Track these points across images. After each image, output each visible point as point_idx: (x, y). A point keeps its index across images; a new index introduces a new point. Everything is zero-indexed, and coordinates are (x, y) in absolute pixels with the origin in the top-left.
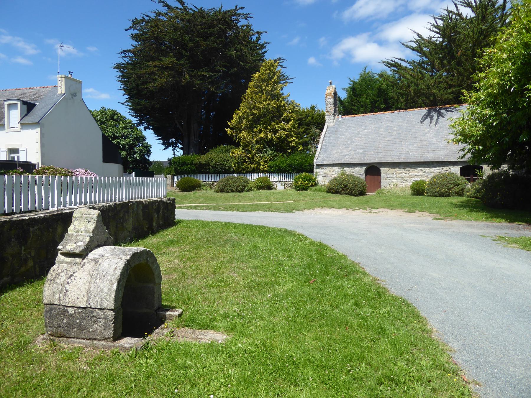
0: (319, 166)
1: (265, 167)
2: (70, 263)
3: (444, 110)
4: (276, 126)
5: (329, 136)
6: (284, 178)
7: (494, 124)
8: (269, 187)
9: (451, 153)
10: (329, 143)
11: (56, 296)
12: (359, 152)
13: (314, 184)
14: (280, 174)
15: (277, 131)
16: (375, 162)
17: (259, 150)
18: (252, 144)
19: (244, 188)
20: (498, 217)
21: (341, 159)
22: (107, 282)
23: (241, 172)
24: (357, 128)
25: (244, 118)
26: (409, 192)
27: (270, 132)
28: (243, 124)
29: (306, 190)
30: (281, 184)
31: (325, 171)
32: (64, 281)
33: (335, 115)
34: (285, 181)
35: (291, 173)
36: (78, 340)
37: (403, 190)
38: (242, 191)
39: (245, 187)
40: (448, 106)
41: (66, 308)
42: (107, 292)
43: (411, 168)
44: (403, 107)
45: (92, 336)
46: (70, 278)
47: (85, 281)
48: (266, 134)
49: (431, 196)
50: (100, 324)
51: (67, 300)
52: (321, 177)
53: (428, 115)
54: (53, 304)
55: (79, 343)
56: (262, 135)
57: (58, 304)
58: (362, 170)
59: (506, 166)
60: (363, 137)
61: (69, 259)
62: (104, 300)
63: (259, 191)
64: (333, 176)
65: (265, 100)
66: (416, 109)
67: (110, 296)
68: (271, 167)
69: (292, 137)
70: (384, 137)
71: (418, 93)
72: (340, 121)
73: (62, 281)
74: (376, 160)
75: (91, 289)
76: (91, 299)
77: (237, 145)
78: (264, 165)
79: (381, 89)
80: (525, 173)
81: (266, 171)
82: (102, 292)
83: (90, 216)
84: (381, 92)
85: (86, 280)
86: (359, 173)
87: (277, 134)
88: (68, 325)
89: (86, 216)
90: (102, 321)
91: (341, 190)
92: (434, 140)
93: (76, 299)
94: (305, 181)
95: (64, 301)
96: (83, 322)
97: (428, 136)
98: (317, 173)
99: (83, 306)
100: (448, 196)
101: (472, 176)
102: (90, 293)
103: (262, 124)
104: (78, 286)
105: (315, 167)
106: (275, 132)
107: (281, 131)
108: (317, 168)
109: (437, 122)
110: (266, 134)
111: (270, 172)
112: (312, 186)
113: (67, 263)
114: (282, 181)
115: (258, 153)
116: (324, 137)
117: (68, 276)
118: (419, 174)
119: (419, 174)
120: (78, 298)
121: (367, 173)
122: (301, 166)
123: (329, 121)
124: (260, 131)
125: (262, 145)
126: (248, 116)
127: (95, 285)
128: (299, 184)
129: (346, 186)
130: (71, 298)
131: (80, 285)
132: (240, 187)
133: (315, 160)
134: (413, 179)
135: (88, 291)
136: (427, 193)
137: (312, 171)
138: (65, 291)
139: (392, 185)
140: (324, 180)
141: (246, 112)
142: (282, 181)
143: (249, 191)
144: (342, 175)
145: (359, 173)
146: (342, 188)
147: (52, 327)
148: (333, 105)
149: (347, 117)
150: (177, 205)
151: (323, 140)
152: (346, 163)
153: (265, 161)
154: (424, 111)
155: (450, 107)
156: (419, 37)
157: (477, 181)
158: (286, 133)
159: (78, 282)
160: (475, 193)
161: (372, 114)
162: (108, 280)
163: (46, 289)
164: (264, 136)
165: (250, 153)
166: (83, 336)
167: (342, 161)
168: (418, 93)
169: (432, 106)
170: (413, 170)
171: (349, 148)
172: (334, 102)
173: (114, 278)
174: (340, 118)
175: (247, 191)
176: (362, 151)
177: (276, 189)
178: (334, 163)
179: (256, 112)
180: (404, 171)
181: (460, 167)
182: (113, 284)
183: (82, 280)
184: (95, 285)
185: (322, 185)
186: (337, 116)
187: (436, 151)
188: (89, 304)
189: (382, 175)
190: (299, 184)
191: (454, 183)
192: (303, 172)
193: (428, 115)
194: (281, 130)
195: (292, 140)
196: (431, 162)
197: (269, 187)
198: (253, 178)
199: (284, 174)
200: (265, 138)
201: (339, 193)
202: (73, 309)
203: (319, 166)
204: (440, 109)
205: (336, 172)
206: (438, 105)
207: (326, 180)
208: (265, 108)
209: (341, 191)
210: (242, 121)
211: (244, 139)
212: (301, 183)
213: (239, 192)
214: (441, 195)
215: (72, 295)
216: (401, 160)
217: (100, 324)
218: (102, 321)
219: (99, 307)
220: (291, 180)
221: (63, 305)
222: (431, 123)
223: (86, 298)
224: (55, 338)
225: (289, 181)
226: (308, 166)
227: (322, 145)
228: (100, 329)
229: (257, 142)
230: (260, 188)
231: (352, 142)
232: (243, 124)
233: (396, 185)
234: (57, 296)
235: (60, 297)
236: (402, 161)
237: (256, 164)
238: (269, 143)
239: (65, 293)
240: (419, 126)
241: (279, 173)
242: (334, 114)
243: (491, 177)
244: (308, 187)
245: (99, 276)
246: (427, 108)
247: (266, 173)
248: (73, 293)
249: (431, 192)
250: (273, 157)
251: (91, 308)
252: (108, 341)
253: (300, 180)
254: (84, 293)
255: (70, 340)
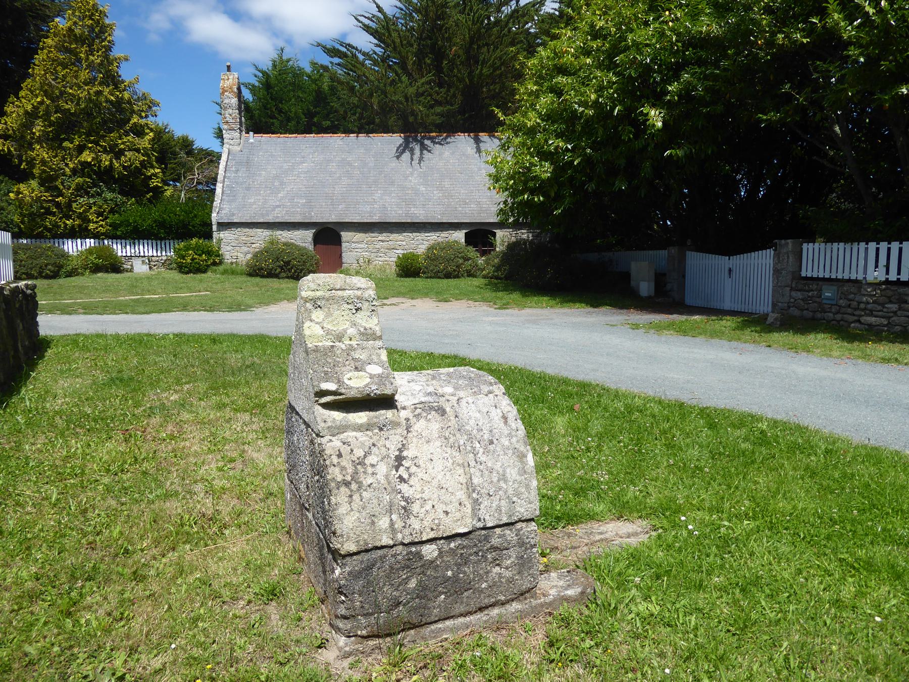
0: (223, 226)
1: (101, 226)
2: (368, 427)
3: (429, 141)
4: (120, 142)
5: (234, 169)
6: (146, 249)
7: (575, 163)
8: (115, 266)
9: (450, 209)
10: (237, 183)
11: (381, 523)
12: (299, 203)
13: (218, 262)
14: (136, 241)
15: (121, 153)
16: (331, 220)
17: (81, 190)
18: (64, 174)
19: (58, 271)
20: (574, 301)
21: (268, 215)
22: (505, 454)
23: (40, 236)
24: (286, 159)
25: (37, 117)
26: (392, 270)
27: (105, 151)
28: (38, 128)
29: (205, 272)
30: (143, 262)
31: (236, 236)
32: (387, 477)
33: (241, 131)
34: (151, 254)
35: (161, 239)
36: (448, 623)
37: (382, 270)
38: (55, 275)
39: (61, 267)
40: (434, 134)
41: (414, 549)
42: (518, 478)
43: (392, 232)
44: (356, 129)
45: (486, 601)
46: (400, 465)
47: (449, 465)
48: (97, 156)
49: (431, 277)
50: (509, 562)
51: (416, 524)
52: (229, 248)
53: (405, 147)
54: (377, 548)
55: (452, 630)
56: (87, 156)
57: (391, 543)
58: (309, 234)
59: (525, 231)
60: (302, 176)
61: (361, 417)
62: (515, 499)
63: (95, 276)
64: (254, 246)
65: (91, 82)
66: (385, 135)
67: (527, 487)
68: (114, 226)
69: (153, 167)
70: (340, 178)
71: (386, 109)
72: (252, 143)
73: (381, 477)
74: (333, 218)
75: (476, 481)
76: (482, 506)
77: (24, 176)
78: (97, 222)
79: (320, 92)
80: (549, 242)
81: (103, 234)
82: (506, 481)
83: (359, 293)
84: (320, 98)
85: (451, 461)
86: (304, 239)
87: (123, 158)
88: (423, 592)
89: (340, 293)
90: (513, 553)
91: (279, 270)
92: (422, 189)
93: (442, 516)
94: (200, 255)
95: (407, 532)
96: (465, 573)
97: (411, 181)
98: (220, 240)
99: (466, 530)
100: (457, 277)
101: (480, 246)
102: (474, 491)
103: (85, 133)
104: (435, 483)
105: (214, 228)
106: (119, 154)
107: (131, 153)
108: (219, 230)
109: (421, 159)
110: (97, 156)
111: (114, 237)
112: (214, 264)
113: (359, 428)
114: (142, 254)
115: (81, 197)
116: (225, 172)
117: (392, 461)
118: (404, 243)
119: (404, 243)
120: (447, 513)
121: (317, 240)
122: (185, 226)
123: (232, 142)
124: (81, 149)
125: (87, 180)
126: (47, 114)
127: (481, 467)
128: (189, 261)
129: (287, 263)
130: (429, 519)
131: (440, 477)
132: (50, 267)
133: (214, 215)
134: (395, 251)
135: (470, 487)
136: (424, 273)
137: (208, 236)
138: (403, 503)
139: (361, 260)
140: (236, 254)
141: (42, 103)
142: (142, 254)
143: (70, 276)
144: (272, 243)
145: (304, 239)
146: (281, 268)
147: (372, 614)
148: (237, 111)
149: (265, 137)
150: (42, 302)
151: (225, 177)
152: (277, 221)
153: (99, 214)
154: (397, 139)
155: (437, 136)
156: (379, 11)
157: (492, 252)
158: (142, 158)
159: (430, 471)
160: (494, 272)
161: (312, 135)
162: (505, 449)
163: (342, 510)
164: (93, 159)
165: (61, 194)
166: (462, 609)
167: (270, 218)
168: (386, 109)
169: (411, 132)
170: (395, 236)
171: (280, 195)
172: (238, 105)
173: (518, 441)
174: (252, 138)
175: (66, 276)
176: (304, 201)
177: (131, 270)
178: (255, 221)
179: (70, 106)
180: (380, 238)
181: (464, 231)
182: (522, 457)
183: (439, 464)
184: (481, 467)
185: (232, 263)
186: (244, 132)
187: (427, 206)
188: (479, 520)
189: (344, 245)
190: (189, 261)
191: (463, 257)
192: (191, 237)
193: (405, 147)
194: (130, 150)
195: (153, 175)
196: (422, 223)
197: (115, 266)
198: (72, 247)
199: (145, 241)
200: (95, 165)
201: (277, 276)
202: (434, 547)
203: (223, 226)
204: (423, 138)
205: (261, 238)
206: (420, 131)
207: (239, 254)
208: (90, 98)
209: (280, 272)
210: (32, 124)
211: (43, 162)
212: (193, 259)
213: (47, 277)
214: (448, 276)
215: (428, 507)
216: (376, 219)
217: (509, 562)
218: (513, 553)
219: (505, 520)
220: (164, 253)
221: (406, 541)
222: (412, 159)
223: (469, 506)
224: (381, 641)
225: (159, 254)
226: (200, 225)
227: (223, 186)
228: (508, 574)
229: (74, 172)
230: (96, 269)
231: (282, 183)
232: (38, 128)
233: (369, 261)
234: (384, 523)
235: (392, 524)
236: (377, 221)
237: (78, 217)
238: (105, 176)
239: (404, 508)
240: (394, 163)
241: (134, 239)
242: (239, 128)
243: (513, 247)
244: (208, 266)
245: (478, 445)
246: (402, 135)
247: (103, 239)
248: (430, 503)
249: (432, 271)
250: (117, 205)
251: (484, 528)
252: (526, 599)
253: (191, 252)
254: (461, 495)
255: (427, 630)
